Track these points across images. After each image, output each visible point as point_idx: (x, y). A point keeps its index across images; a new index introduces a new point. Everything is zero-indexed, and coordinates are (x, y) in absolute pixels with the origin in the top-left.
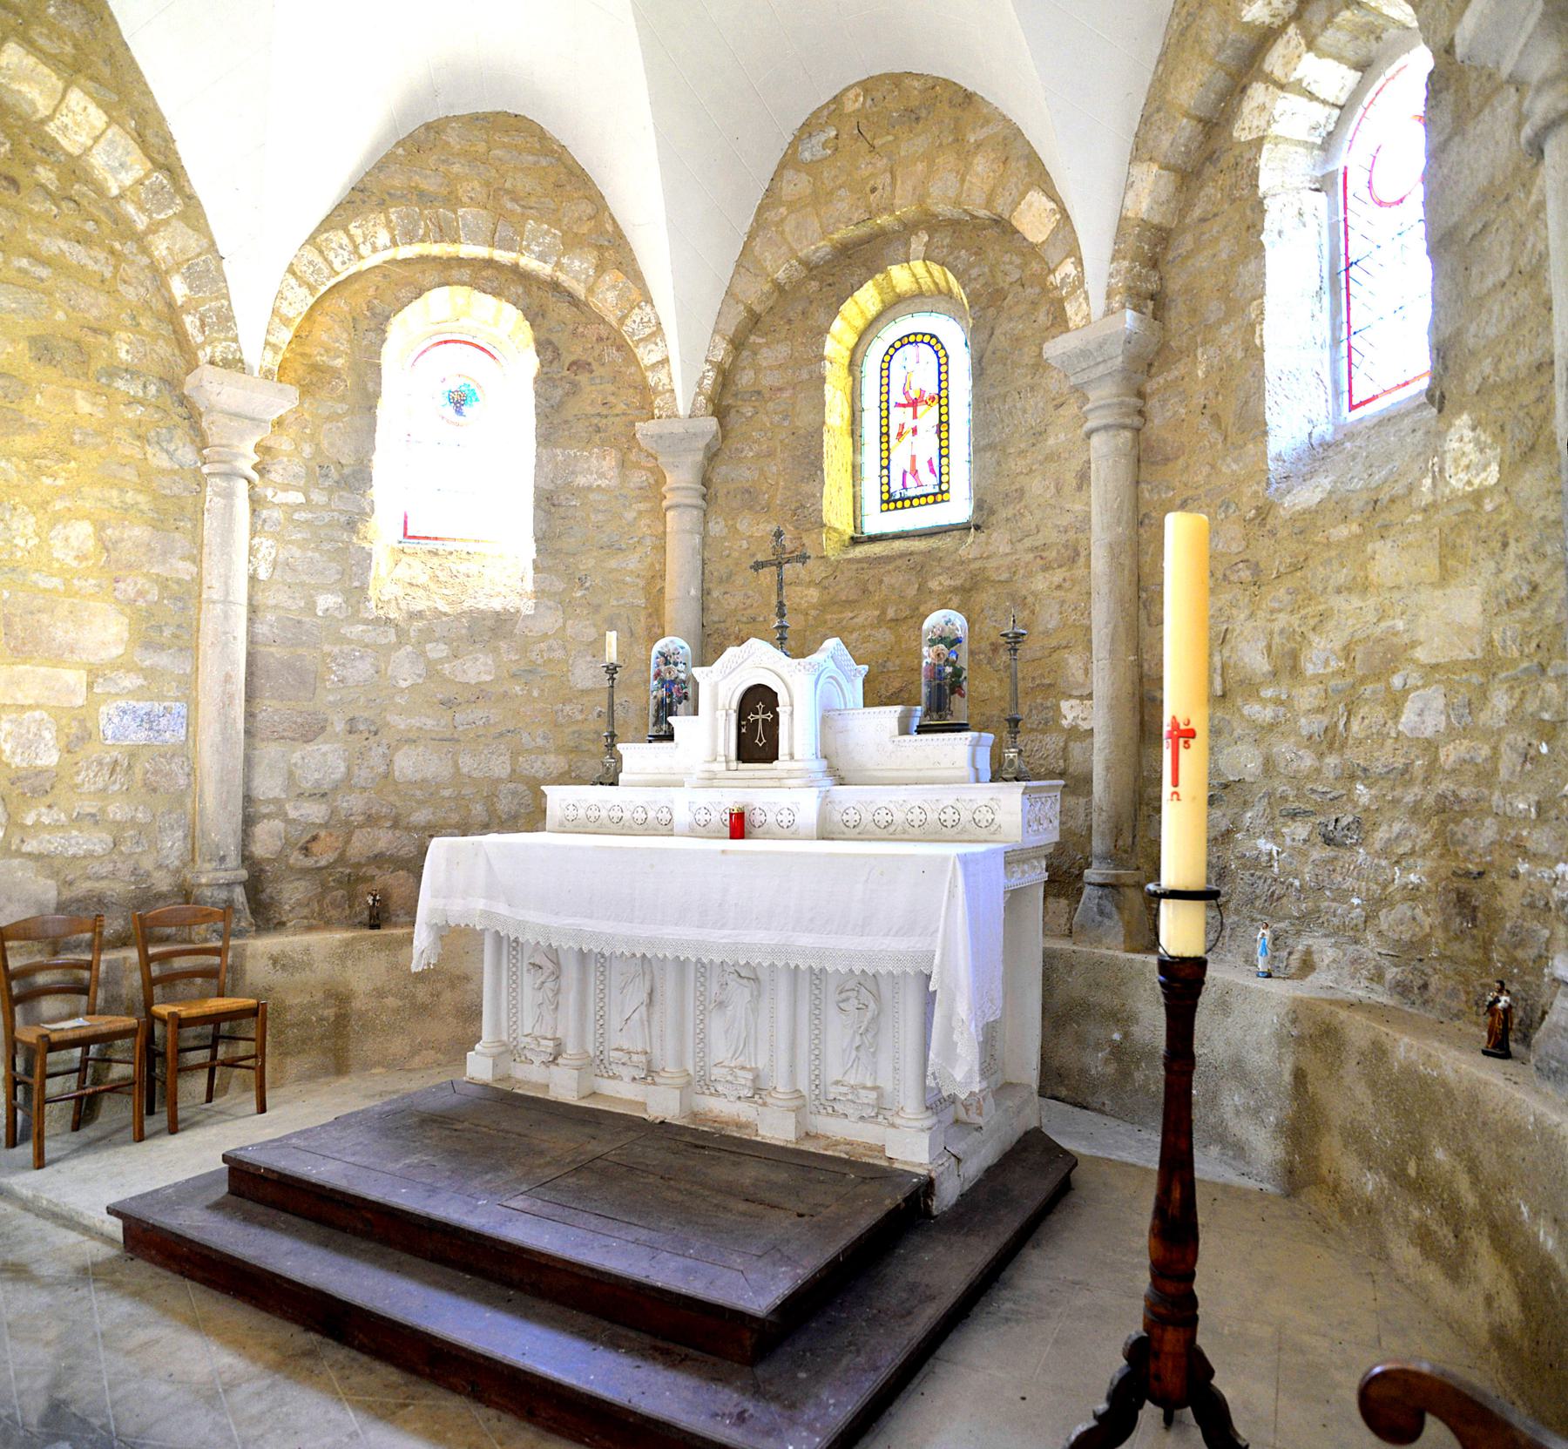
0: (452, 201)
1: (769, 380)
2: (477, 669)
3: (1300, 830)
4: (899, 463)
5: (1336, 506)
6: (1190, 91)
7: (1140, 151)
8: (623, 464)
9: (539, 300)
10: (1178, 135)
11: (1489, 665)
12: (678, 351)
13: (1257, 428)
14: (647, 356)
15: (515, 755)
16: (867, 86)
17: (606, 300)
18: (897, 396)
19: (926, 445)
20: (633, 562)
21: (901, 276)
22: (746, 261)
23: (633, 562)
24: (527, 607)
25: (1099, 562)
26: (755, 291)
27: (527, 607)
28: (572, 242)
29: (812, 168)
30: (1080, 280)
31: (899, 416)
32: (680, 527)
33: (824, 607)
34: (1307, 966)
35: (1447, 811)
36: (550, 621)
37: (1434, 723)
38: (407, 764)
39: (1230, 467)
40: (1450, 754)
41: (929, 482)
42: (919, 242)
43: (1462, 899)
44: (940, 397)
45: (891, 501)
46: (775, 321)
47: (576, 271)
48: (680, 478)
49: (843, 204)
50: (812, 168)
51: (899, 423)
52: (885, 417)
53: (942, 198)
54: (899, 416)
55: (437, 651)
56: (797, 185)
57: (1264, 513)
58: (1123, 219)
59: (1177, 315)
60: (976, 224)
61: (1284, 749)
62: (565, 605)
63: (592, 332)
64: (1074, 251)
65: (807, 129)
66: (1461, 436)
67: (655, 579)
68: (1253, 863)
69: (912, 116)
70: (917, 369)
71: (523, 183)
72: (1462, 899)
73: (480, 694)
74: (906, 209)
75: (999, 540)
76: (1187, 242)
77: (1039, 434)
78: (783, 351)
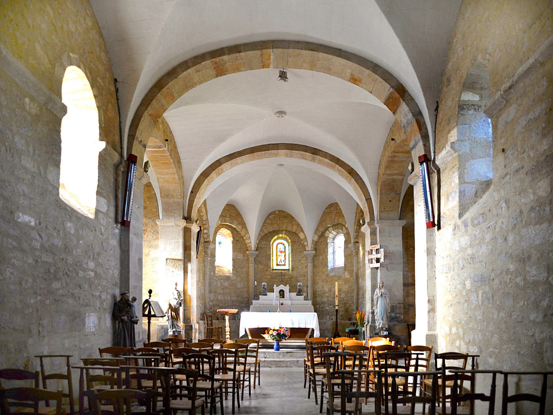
0: (226, 217)
1: (263, 246)
2: (226, 284)
3: (332, 306)
4: (279, 260)
5: (335, 276)
6: (321, 229)
7: (315, 233)
8: (243, 255)
9: (234, 232)
10: (319, 234)
11: (348, 292)
12: (252, 240)
13: (328, 267)
14: (247, 241)
15: (231, 296)
16: (279, 211)
17: (243, 233)
18: (278, 251)
19: (283, 258)
20: (245, 270)
21: (280, 235)
22: (261, 230)
23: (245, 270)
24: (231, 275)
25: (309, 278)
26: (263, 234)
27: (231, 275)
28: (239, 224)
29: (271, 219)
30: (307, 245)
31: (279, 253)
32: (252, 266)
33: (271, 279)
34: (332, 319)
35: (345, 304)
36: (235, 278)
37: (344, 296)
38: (219, 297)
39: (324, 269)
40: (345, 299)
41: (283, 263)
42: (284, 232)
43: (346, 311)
44: (285, 252)
45: (278, 265)
46: (265, 238)
47: (239, 228)
48: (251, 259)
49: (276, 226)
50: (271, 219)
51: (281, 255)
52: (277, 253)
53: (289, 229)
54: (279, 253)
55: (222, 281)
56: (269, 221)
57: (328, 275)
58: (313, 240)
59: (318, 251)
60: (292, 232)
61: (330, 298)
62: (237, 275)
63: (239, 236)
64: (307, 241)
65: (270, 214)
66: (346, 273)
67: (248, 273)
68: (326, 310)
69: (285, 217)
70: (281, 247)
71: (233, 215)
72: (346, 311)
73: (226, 288)
74: (284, 229)
75: (295, 273)
76: (319, 244)
77: (300, 261)
78: (265, 242)
